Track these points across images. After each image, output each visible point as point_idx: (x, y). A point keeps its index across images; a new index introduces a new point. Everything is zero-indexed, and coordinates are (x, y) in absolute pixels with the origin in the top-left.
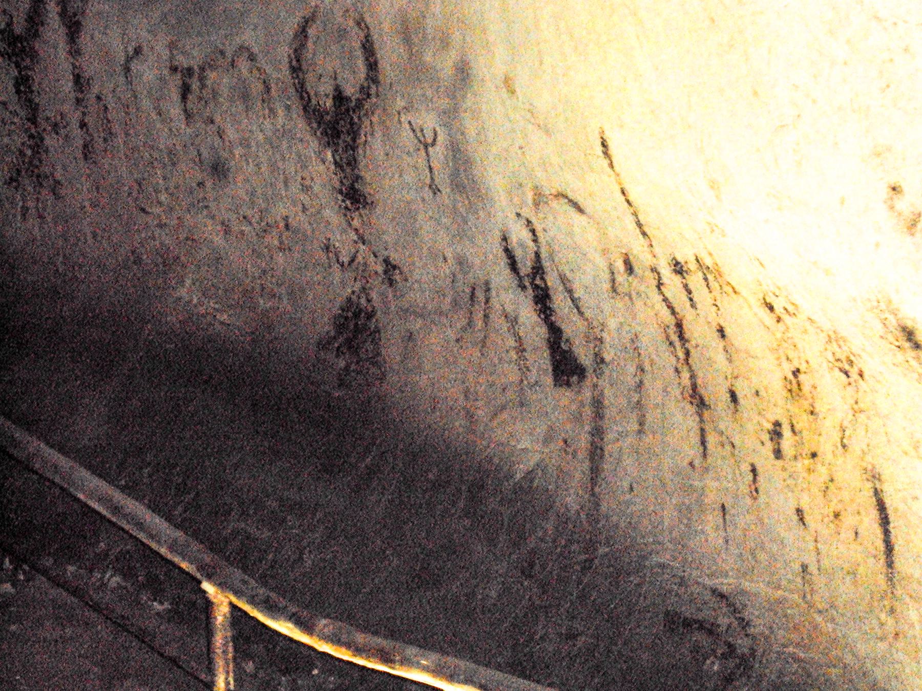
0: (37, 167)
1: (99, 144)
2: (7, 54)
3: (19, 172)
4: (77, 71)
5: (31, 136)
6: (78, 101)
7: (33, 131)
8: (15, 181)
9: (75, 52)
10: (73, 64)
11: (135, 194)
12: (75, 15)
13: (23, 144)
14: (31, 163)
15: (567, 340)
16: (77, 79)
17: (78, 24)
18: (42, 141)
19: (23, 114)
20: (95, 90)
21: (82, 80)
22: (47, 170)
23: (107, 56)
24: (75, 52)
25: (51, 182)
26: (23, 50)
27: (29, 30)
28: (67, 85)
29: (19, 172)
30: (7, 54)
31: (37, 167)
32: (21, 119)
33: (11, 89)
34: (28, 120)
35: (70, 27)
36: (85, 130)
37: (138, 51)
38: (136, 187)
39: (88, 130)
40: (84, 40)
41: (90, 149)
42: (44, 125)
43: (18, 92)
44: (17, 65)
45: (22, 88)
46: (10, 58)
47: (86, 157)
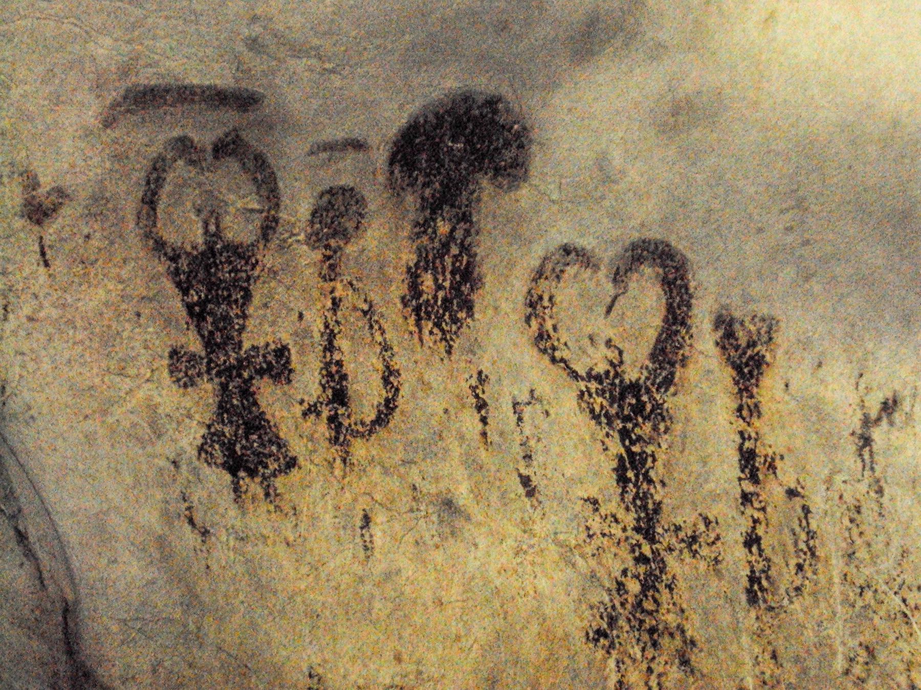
0: (650, 613)
1: (785, 576)
2: (607, 415)
3: (612, 621)
4: (748, 445)
5: (642, 559)
6: (746, 498)
7: (646, 549)
8: (606, 636)
9: (747, 409)
10: (741, 433)
11: (858, 670)
12: (752, 344)
13: (624, 572)
14: (639, 605)
15: (275, 425)
16: (747, 458)
17: (758, 362)
18: (662, 571)
19: (630, 519)
20: (787, 475)
21: (759, 462)
22: (672, 619)
23: (816, 413)
24: (747, 409)
25: (678, 641)
26: (639, 409)
27: (653, 373)
28: (727, 470)
29: (612, 621)
30: (607, 415)
31: (650, 613)
32: (624, 530)
33: (610, 480)
34: (637, 529)
35: (738, 368)
36: (754, 549)
37: (889, 407)
38: (863, 656)
39: (761, 550)
40: (770, 389)
41: (765, 583)
42: (669, 539)
43: (622, 480)
44: (624, 434)
45: (630, 474)
46: (610, 423)
47: (753, 599)
